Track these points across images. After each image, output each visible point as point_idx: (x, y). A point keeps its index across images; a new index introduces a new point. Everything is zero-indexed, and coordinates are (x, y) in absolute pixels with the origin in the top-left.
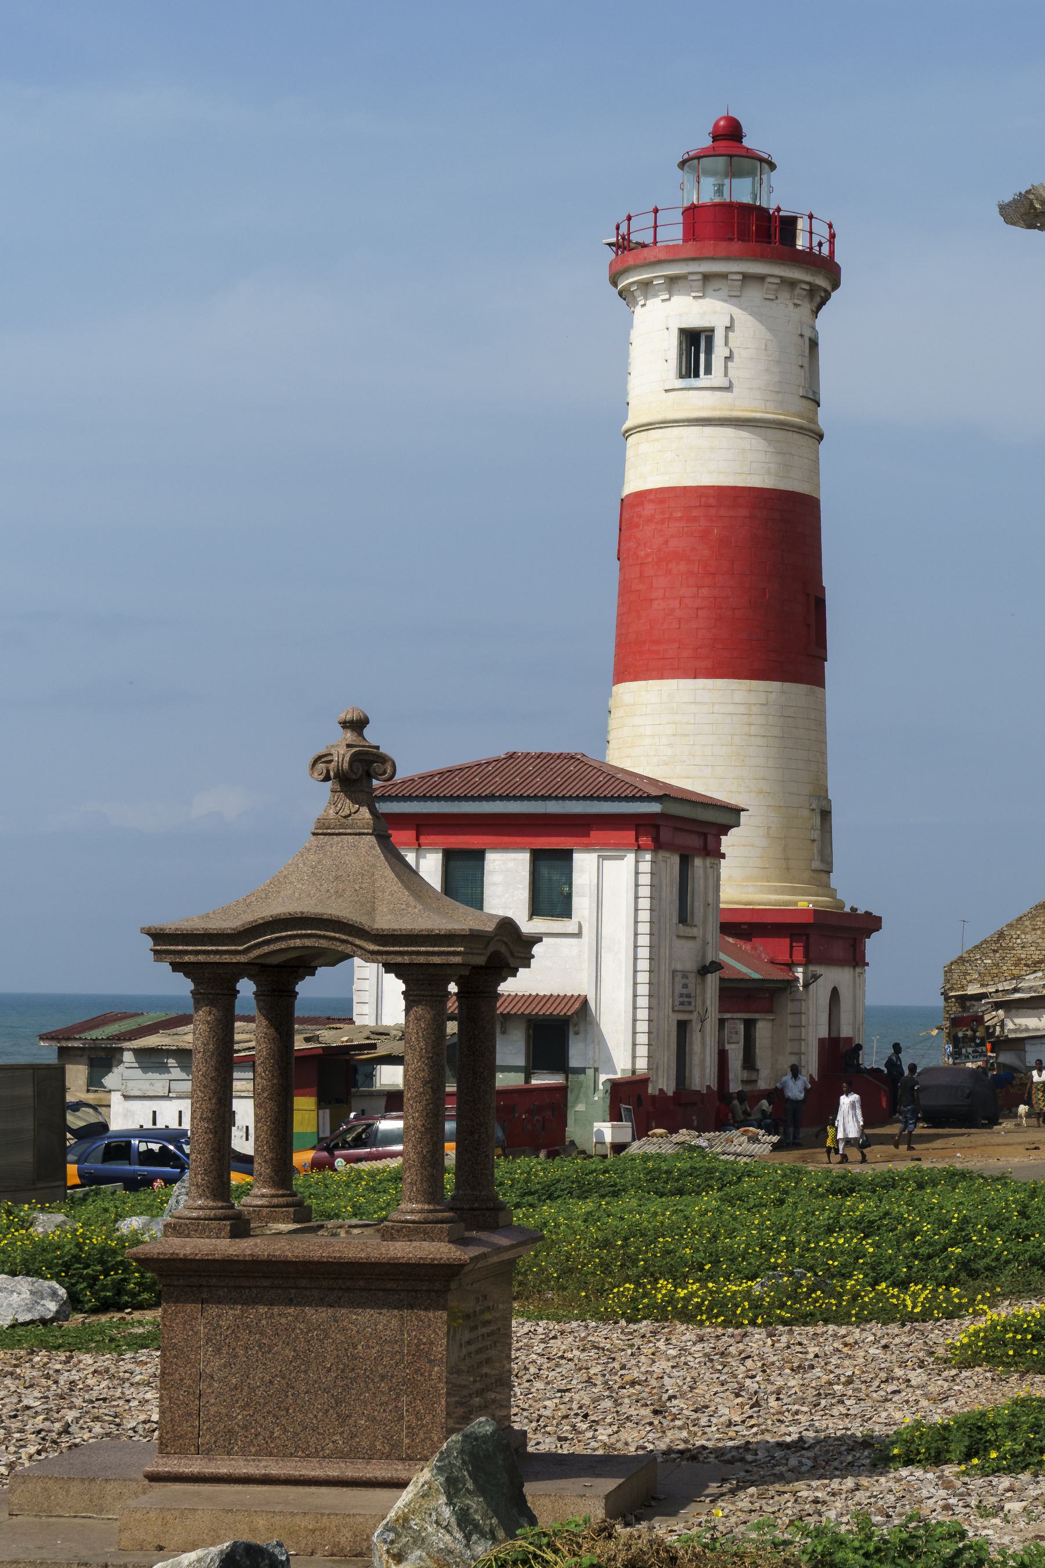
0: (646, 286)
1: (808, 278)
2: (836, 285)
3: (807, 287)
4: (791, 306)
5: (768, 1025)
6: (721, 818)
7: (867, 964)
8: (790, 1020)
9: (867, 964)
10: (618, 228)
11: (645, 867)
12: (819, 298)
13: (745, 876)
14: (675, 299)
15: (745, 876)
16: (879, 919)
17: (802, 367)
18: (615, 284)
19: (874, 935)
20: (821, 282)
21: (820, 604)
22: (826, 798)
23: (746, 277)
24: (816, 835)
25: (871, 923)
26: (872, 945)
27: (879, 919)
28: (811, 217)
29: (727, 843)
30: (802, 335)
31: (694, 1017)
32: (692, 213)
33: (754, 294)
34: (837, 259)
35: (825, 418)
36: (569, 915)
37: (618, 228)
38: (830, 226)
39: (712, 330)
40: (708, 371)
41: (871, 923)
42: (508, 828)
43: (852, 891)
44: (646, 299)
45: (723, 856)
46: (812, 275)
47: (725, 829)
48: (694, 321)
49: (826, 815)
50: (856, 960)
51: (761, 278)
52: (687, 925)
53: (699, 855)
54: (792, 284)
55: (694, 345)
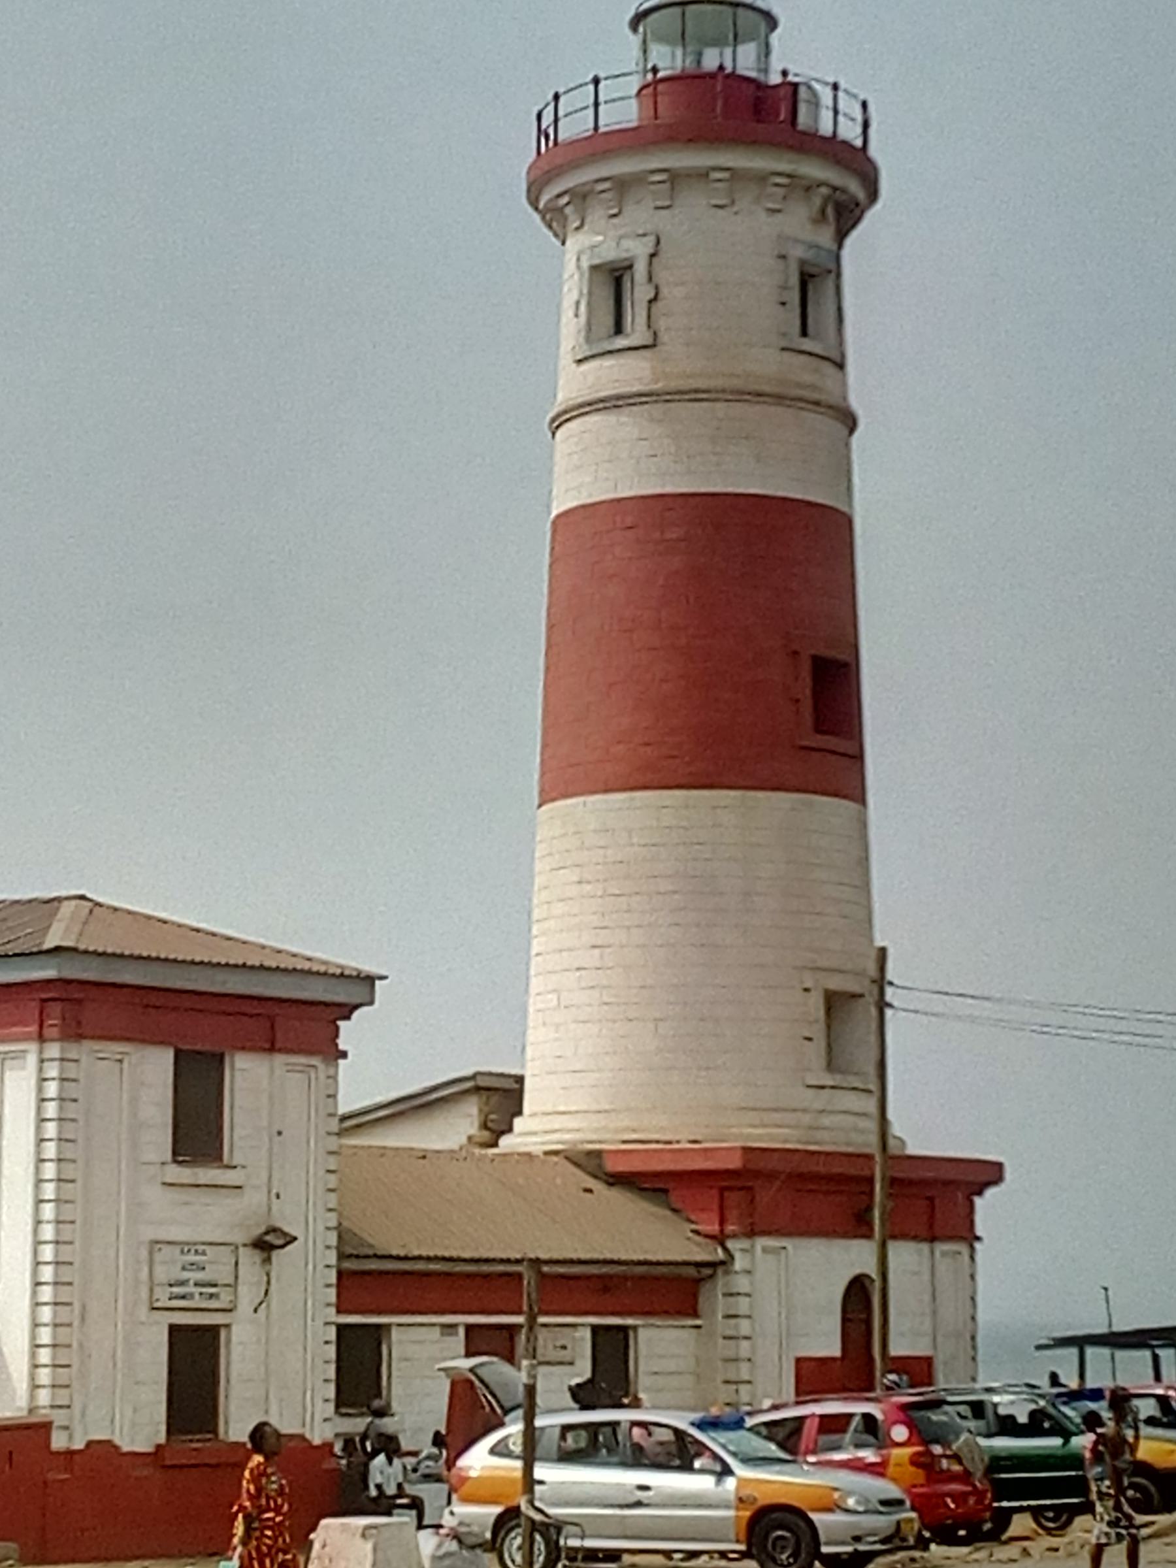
1: (784, 166)
2: (873, 195)
4: (763, 216)
6: (340, 995)
8: (723, 1327)
9: (344, 1055)
10: (539, 117)
16: (999, 1166)
20: (855, 188)
25: (989, 1174)
26: (988, 1208)
27: (999, 1166)
28: (835, 87)
30: (783, 257)
32: (654, 87)
34: (873, 151)
37: (539, 117)
38: (864, 105)
43: (924, 1126)
46: (790, 162)
47: (347, 1010)
48: (610, 253)
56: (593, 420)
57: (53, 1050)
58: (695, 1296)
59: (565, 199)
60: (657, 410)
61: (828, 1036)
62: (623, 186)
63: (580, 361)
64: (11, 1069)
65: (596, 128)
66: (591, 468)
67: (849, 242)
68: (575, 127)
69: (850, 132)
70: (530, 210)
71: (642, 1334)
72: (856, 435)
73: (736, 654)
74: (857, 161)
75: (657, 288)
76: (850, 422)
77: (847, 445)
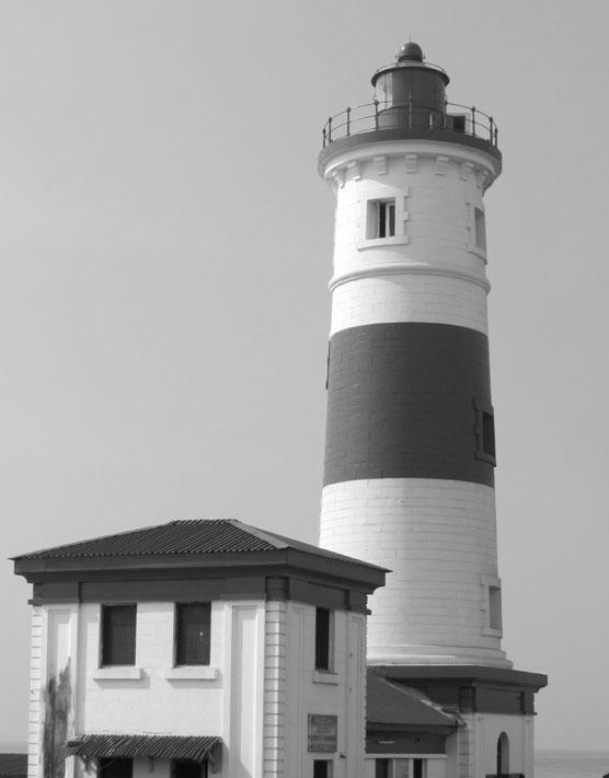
0: (343, 171)
3: (472, 165)
5: (442, 764)
7: (536, 714)
9: (536, 714)
11: (276, 617)
12: (488, 184)
13: (384, 635)
14: (365, 182)
15: (384, 635)
16: (545, 677)
17: (469, 229)
18: (322, 176)
19: (541, 690)
21: (488, 419)
22: (495, 575)
23: (421, 157)
24: (486, 606)
25: (539, 681)
26: (540, 699)
27: (545, 677)
28: (473, 110)
29: (373, 601)
31: (335, 757)
33: (427, 172)
35: (491, 272)
36: (205, 661)
38: (491, 120)
39: (393, 201)
40: (392, 234)
41: (539, 681)
42: (154, 584)
43: (522, 661)
44: (344, 182)
45: (369, 612)
49: (495, 591)
50: (524, 708)
51: (433, 158)
52: (329, 673)
53: (341, 609)
54: (459, 163)
55: (382, 216)
56: (359, 283)
57: (276, 605)
58: (444, 740)
59: (334, 174)
60: (408, 278)
61: (310, 554)
62: (389, 159)
63: (360, 250)
64: (508, 769)
65: (377, 127)
66: (356, 306)
67: (487, 191)
68: (338, 134)
69: (484, 134)
70: (320, 179)
71: (430, 763)
72: (490, 294)
73: (426, 403)
74: (489, 148)
75: (409, 214)
76: (487, 288)
77: (485, 299)
